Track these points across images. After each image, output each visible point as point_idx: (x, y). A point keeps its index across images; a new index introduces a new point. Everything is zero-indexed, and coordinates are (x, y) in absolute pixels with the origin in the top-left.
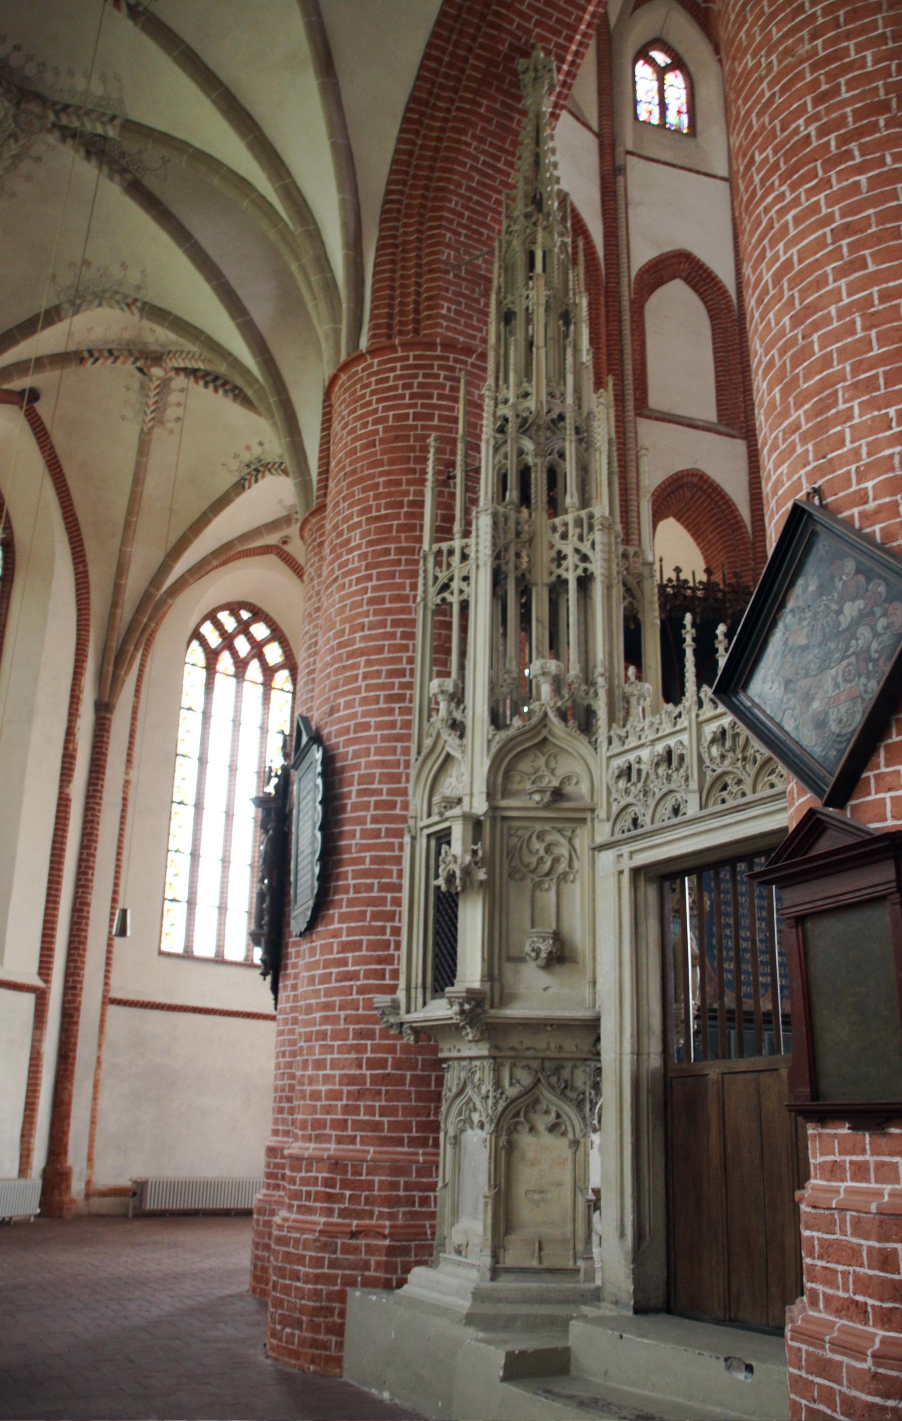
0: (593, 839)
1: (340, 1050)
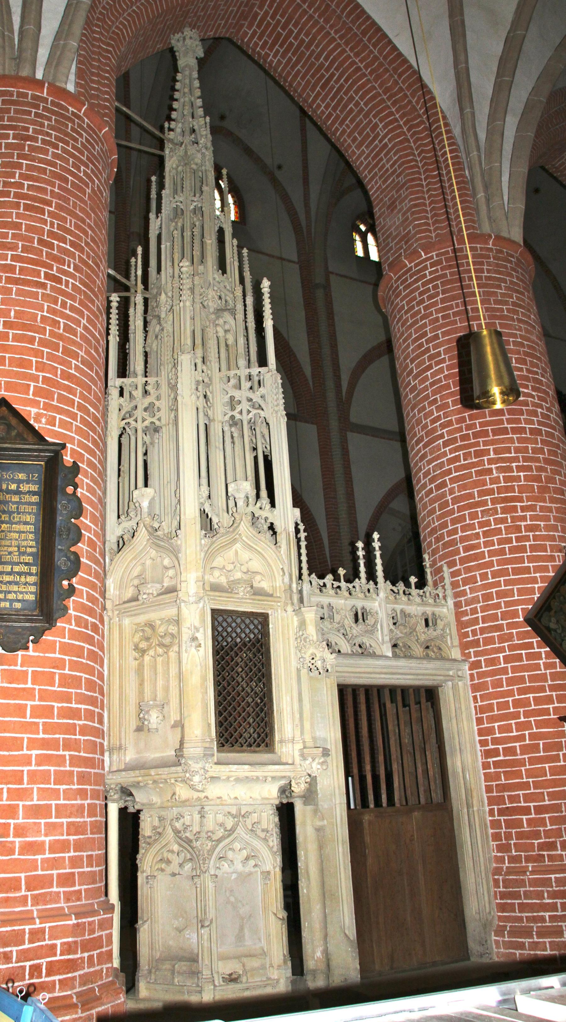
0: (294, 262)
1: (68, 795)
